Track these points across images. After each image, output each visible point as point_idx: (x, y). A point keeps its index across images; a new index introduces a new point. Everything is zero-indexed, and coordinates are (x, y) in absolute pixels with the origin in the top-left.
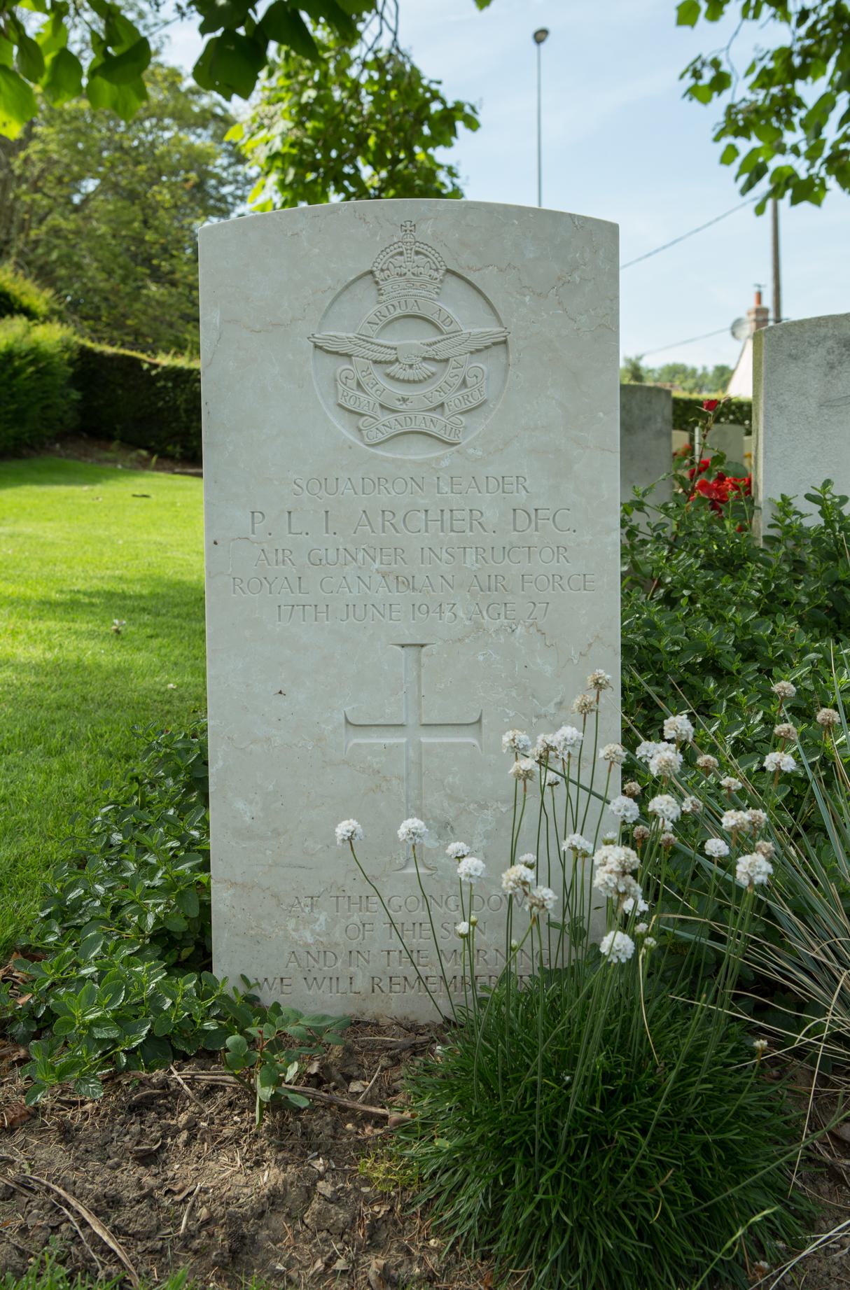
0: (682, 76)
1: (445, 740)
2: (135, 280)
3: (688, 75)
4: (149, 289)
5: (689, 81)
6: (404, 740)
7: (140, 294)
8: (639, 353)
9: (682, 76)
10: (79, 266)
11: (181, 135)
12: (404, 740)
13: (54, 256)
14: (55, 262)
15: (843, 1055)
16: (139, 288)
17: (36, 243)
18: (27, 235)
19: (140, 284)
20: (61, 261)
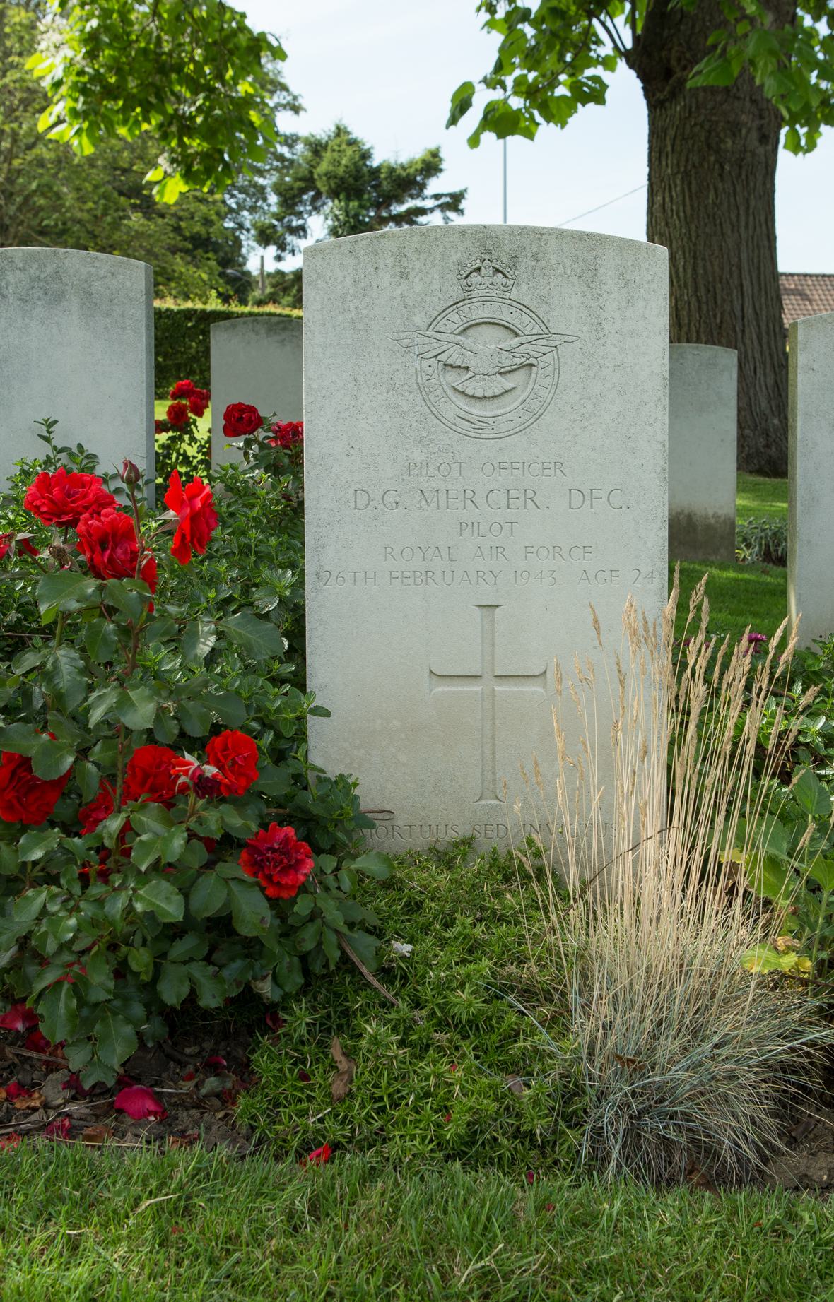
0: (479, 10)
1: (454, 689)
2: (117, 210)
3: (483, 9)
4: (130, 218)
5: (485, 16)
6: (479, 689)
7: (120, 225)
8: (462, 188)
9: (479, 10)
10: (58, 196)
11: (268, 190)
12: (479, 689)
13: (34, 186)
14: (35, 191)
15: (603, 24)
16: (121, 218)
17: (19, 172)
18: (10, 164)
19: (121, 214)
20: (40, 191)
